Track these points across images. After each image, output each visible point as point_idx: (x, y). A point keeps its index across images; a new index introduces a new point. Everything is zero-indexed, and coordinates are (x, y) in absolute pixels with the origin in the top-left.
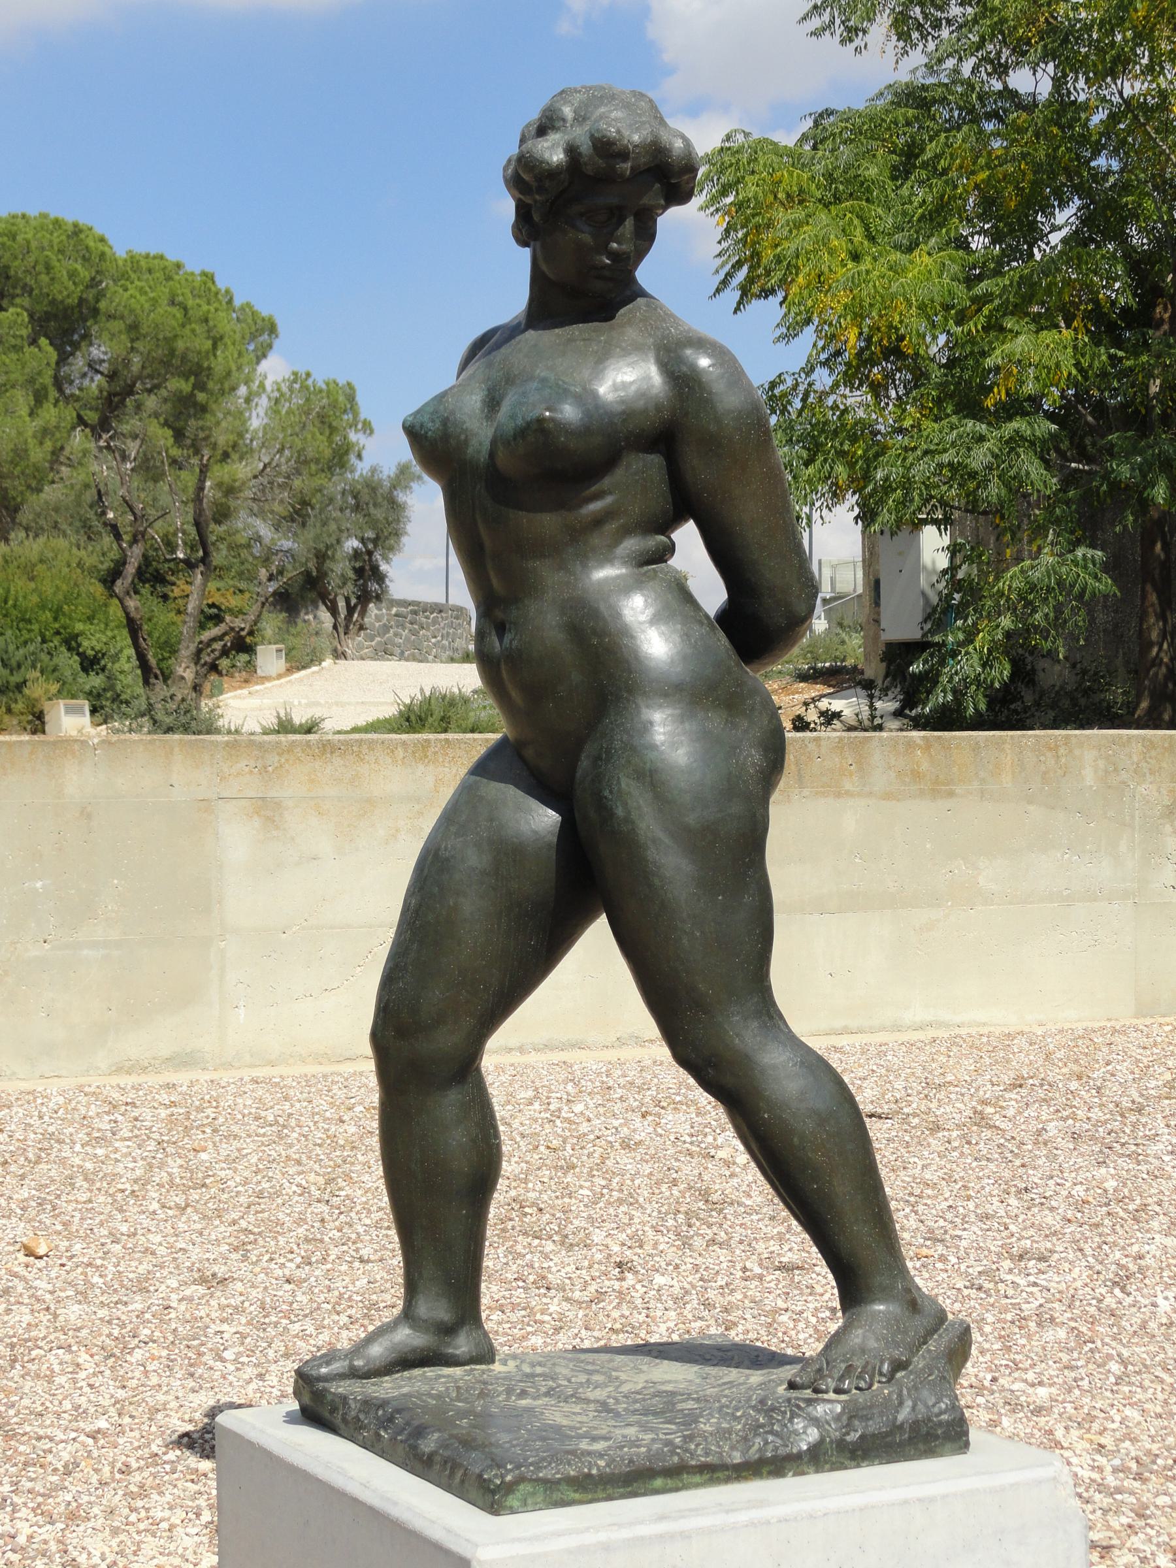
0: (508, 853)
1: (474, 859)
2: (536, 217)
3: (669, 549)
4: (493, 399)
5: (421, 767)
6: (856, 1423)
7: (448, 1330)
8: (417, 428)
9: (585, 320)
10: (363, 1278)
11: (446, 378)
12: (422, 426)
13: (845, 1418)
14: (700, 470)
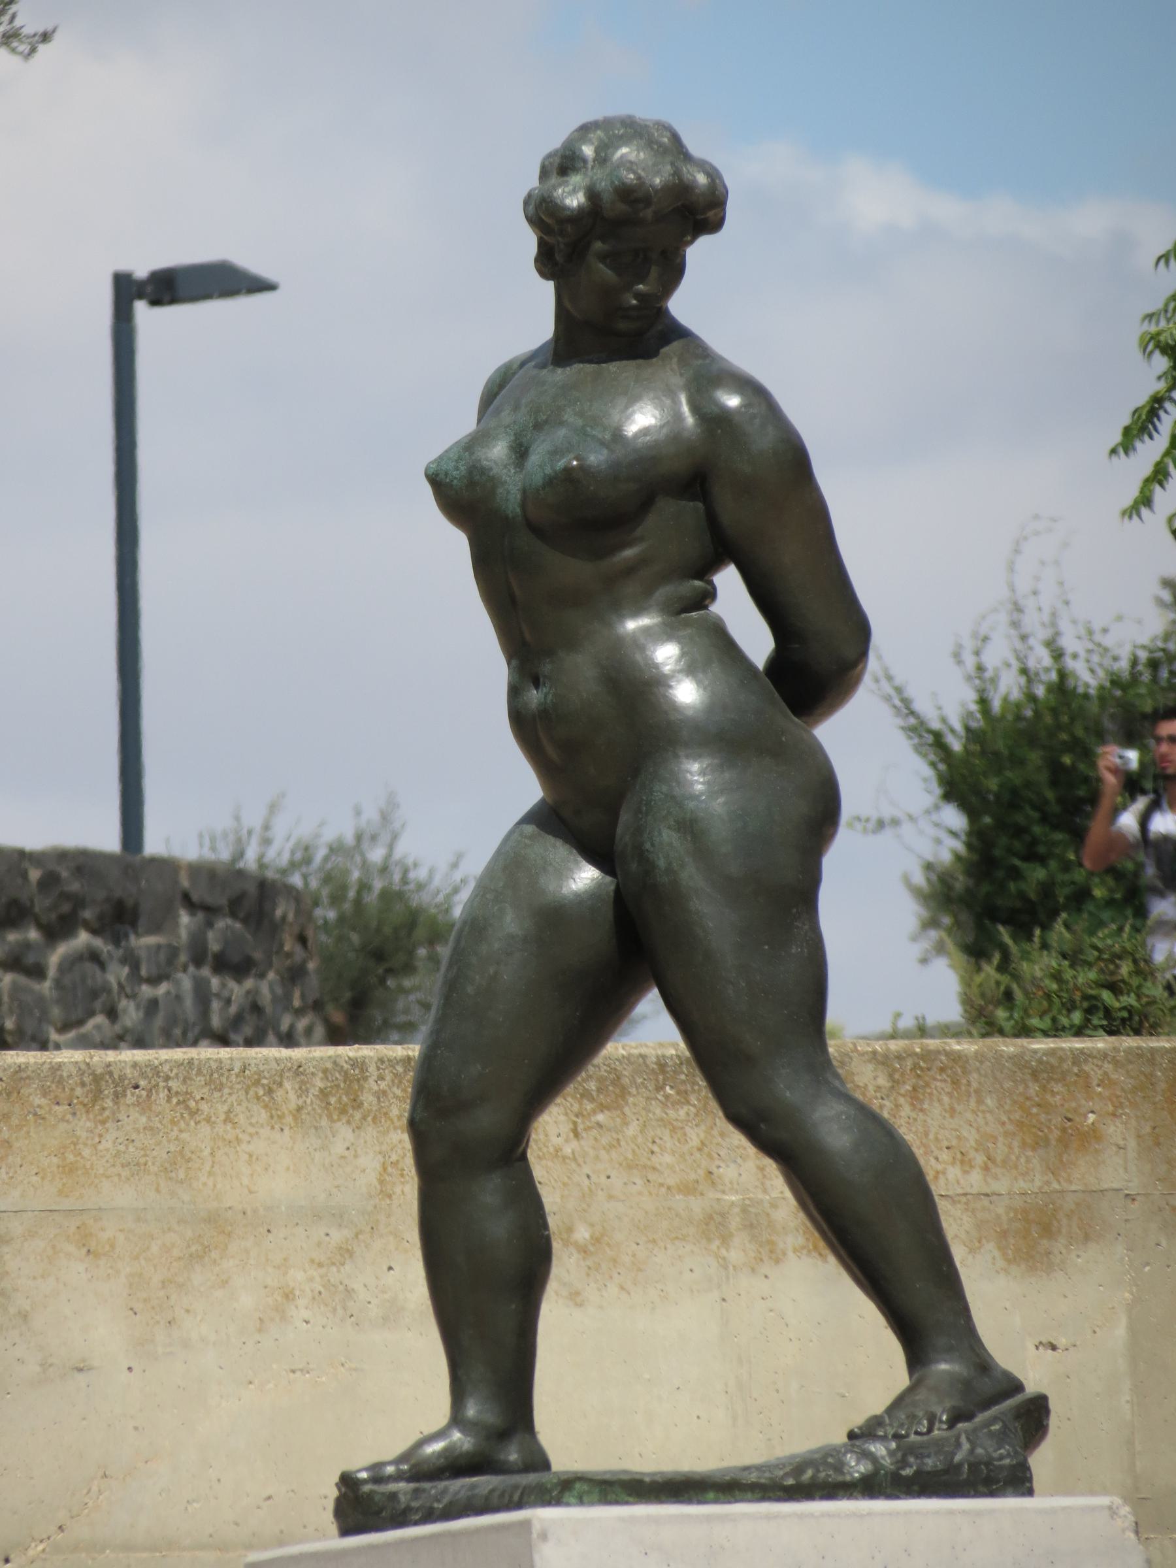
0: (554, 918)
1: (511, 923)
2: (559, 258)
3: (710, 594)
4: (521, 445)
5: (345, 1133)
6: (911, 1459)
7: (502, 1435)
8: (442, 476)
9: (621, 359)
10: (410, 1398)
11: (466, 423)
12: (446, 474)
13: (899, 1455)
14: (733, 512)
